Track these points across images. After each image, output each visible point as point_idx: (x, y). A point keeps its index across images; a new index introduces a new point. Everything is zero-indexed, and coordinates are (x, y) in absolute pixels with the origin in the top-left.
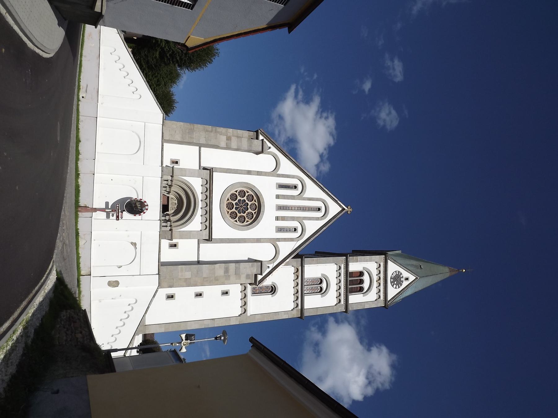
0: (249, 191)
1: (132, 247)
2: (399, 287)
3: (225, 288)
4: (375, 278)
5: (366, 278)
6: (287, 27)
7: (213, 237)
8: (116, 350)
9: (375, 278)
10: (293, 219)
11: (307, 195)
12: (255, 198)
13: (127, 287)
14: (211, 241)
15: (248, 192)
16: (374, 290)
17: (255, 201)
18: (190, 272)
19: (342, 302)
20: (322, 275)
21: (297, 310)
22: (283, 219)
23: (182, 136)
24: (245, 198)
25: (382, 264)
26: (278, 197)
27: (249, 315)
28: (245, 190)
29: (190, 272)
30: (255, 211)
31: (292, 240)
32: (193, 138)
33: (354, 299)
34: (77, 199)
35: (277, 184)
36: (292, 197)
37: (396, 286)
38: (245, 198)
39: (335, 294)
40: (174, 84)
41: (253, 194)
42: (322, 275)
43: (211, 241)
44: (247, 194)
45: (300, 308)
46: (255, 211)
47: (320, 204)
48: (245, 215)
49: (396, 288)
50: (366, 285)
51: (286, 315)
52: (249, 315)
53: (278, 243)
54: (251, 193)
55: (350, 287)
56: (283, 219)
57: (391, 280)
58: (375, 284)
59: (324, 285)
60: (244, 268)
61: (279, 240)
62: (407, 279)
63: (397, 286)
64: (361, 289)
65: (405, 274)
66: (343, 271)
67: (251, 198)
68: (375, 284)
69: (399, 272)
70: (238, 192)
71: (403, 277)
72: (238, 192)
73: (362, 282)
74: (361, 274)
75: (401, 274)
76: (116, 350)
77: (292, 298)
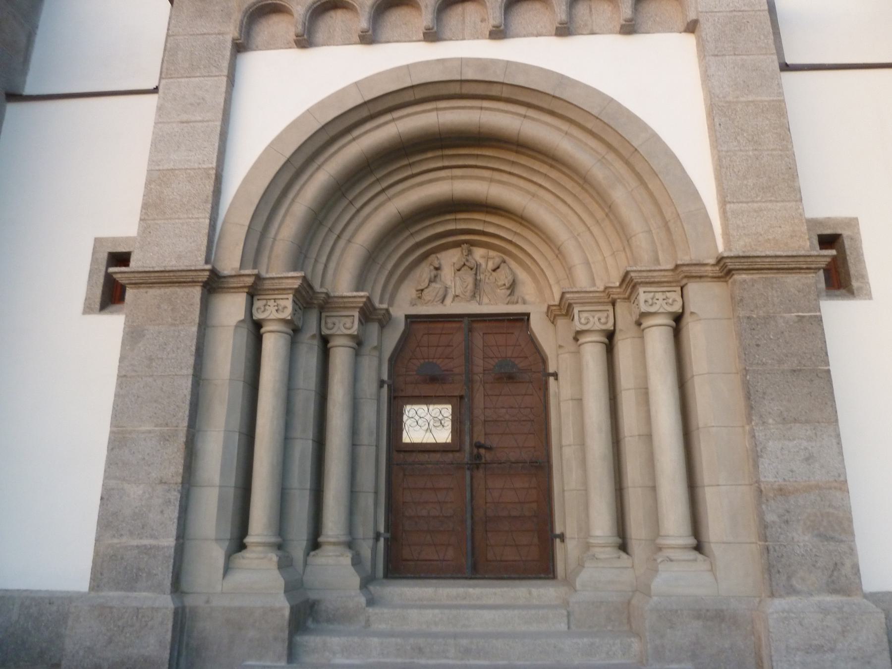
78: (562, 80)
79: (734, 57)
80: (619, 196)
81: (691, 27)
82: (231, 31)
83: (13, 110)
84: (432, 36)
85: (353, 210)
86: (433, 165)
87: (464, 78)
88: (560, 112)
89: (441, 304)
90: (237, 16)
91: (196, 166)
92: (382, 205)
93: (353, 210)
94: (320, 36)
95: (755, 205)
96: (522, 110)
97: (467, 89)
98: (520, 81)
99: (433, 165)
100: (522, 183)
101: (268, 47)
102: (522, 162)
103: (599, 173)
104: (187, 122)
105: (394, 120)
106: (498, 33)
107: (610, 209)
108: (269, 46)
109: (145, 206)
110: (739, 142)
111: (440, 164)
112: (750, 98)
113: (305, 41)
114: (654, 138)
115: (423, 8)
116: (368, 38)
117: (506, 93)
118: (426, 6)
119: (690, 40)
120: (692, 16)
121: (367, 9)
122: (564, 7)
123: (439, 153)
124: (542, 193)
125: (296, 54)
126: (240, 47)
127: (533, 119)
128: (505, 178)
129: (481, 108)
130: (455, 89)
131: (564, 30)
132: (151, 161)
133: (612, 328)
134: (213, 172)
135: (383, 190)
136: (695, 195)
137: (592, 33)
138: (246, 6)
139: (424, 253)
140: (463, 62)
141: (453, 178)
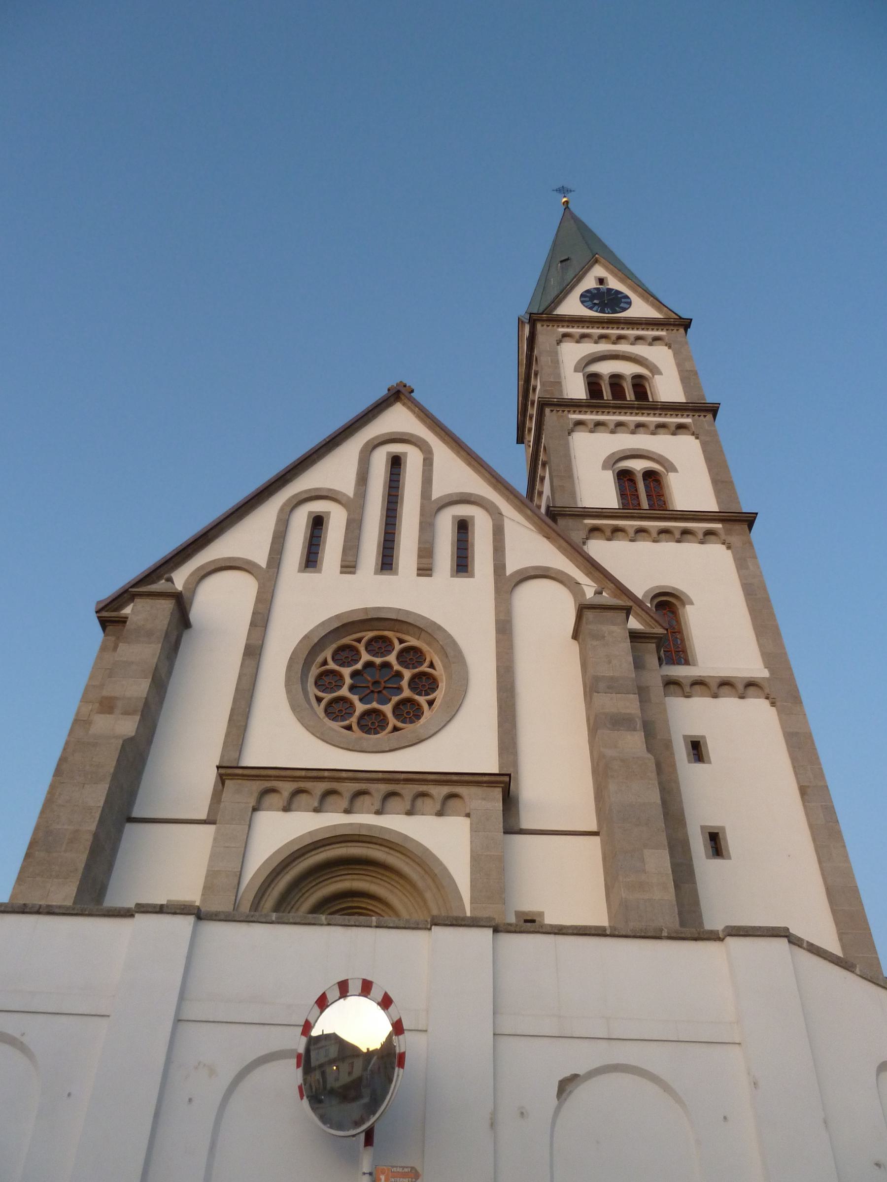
0: (320, 659)
1: (581, 1094)
3: (681, 752)
4: (604, 347)
5: (605, 368)
7: (496, 770)
9: (604, 347)
10: (427, 526)
11: (347, 486)
12: (347, 640)
14: (509, 775)
15: (325, 663)
17: (359, 640)
18: (647, 852)
20: (605, 467)
21: (728, 532)
22: (426, 553)
23: (57, 877)
24: (346, 672)
26: (349, 566)
27: (766, 674)
28: (314, 671)
29: (647, 852)
30: (396, 642)
31: (498, 533)
32: (77, 831)
34: (203, 822)
35: (301, 570)
36: (354, 527)
37: (623, 302)
38: (344, 692)
41: (334, 646)
42: (605, 467)
43: (509, 775)
44: (332, 665)
45: (719, 526)
46: (396, 642)
47: (380, 461)
48: (407, 674)
50: (627, 369)
51: (749, 564)
52: (766, 674)
53: (509, 571)
54: (328, 653)
56: (426, 553)
57: (606, 312)
58: (623, 348)
59: (638, 466)
60: (610, 662)
61: (499, 567)
63: (623, 300)
66: (590, 417)
67: (346, 654)
68: (623, 348)
70: (320, 694)
72: (320, 694)
73: (616, 380)
77: (690, 548)
78: (406, 837)
79: (484, 833)
80: (428, 895)
81: (468, 815)
82: (252, 802)
83: (129, 828)
84: (348, 811)
85: (300, 894)
86: (343, 873)
87: (361, 834)
88: (404, 852)
89: (428, 1030)
90: (256, 795)
91: (231, 870)
92: (315, 892)
93: (300, 894)
94: (294, 806)
95: (484, 905)
96: (387, 850)
97: (361, 839)
98: (387, 837)
99: (343, 873)
100: (386, 885)
101: (268, 809)
102: (388, 874)
103: (420, 884)
104: (227, 847)
105: (325, 851)
106: (378, 812)
107: (425, 901)
108: (269, 809)
109: (204, 888)
110: (480, 874)
111: (346, 872)
112: (488, 853)
113: (287, 809)
114: (445, 869)
115: (344, 798)
116: (317, 810)
117: (379, 841)
118: (346, 797)
119: (467, 821)
120: (468, 811)
121: (318, 796)
122: (410, 803)
123: (346, 867)
124: (396, 890)
125: (281, 814)
126: (255, 809)
127: (392, 855)
128: (378, 881)
129: (368, 848)
130: (357, 838)
131: (410, 813)
132: (209, 865)
133: (164, 911)
134: (238, 874)
135: (317, 884)
136: (460, 898)
137: (423, 814)
138: (260, 789)
139: (380, 1107)
140: (361, 825)
141: (353, 879)
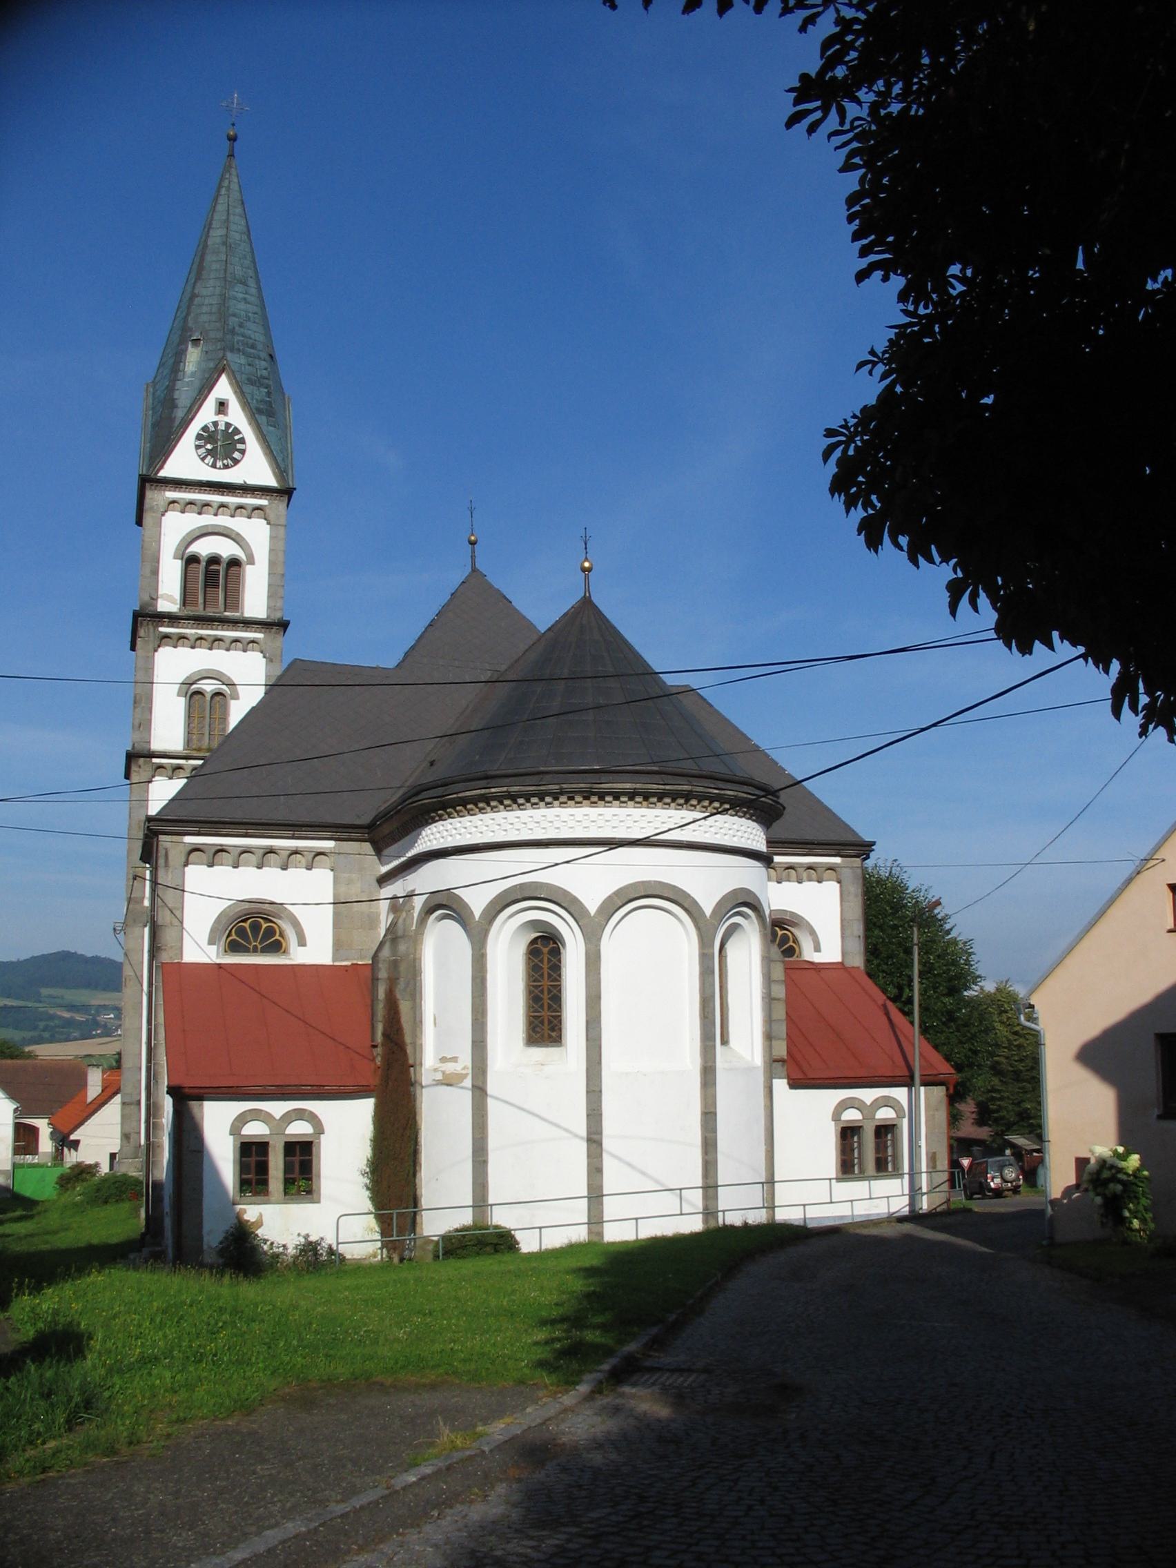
2: (242, 441)
4: (207, 520)
5: (203, 548)
6: (188, 1105)
8: (979, 1199)
13: (435, 1024)
16: (238, 524)
19: (263, 502)
25: (171, 495)
33: (255, 602)
39: (236, 655)
40: (947, 927)
49: (243, 452)
55: (250, 1176)
57: (218, 466)
58: (223, 520)
62: (222, 406)
64: (234, 563)
65: (206, 415)
69: (199, 437)
71: (215, 424)
73: (214, 560)
74: (191, 561)
75: (205, 428)
76: (979, 1199)
